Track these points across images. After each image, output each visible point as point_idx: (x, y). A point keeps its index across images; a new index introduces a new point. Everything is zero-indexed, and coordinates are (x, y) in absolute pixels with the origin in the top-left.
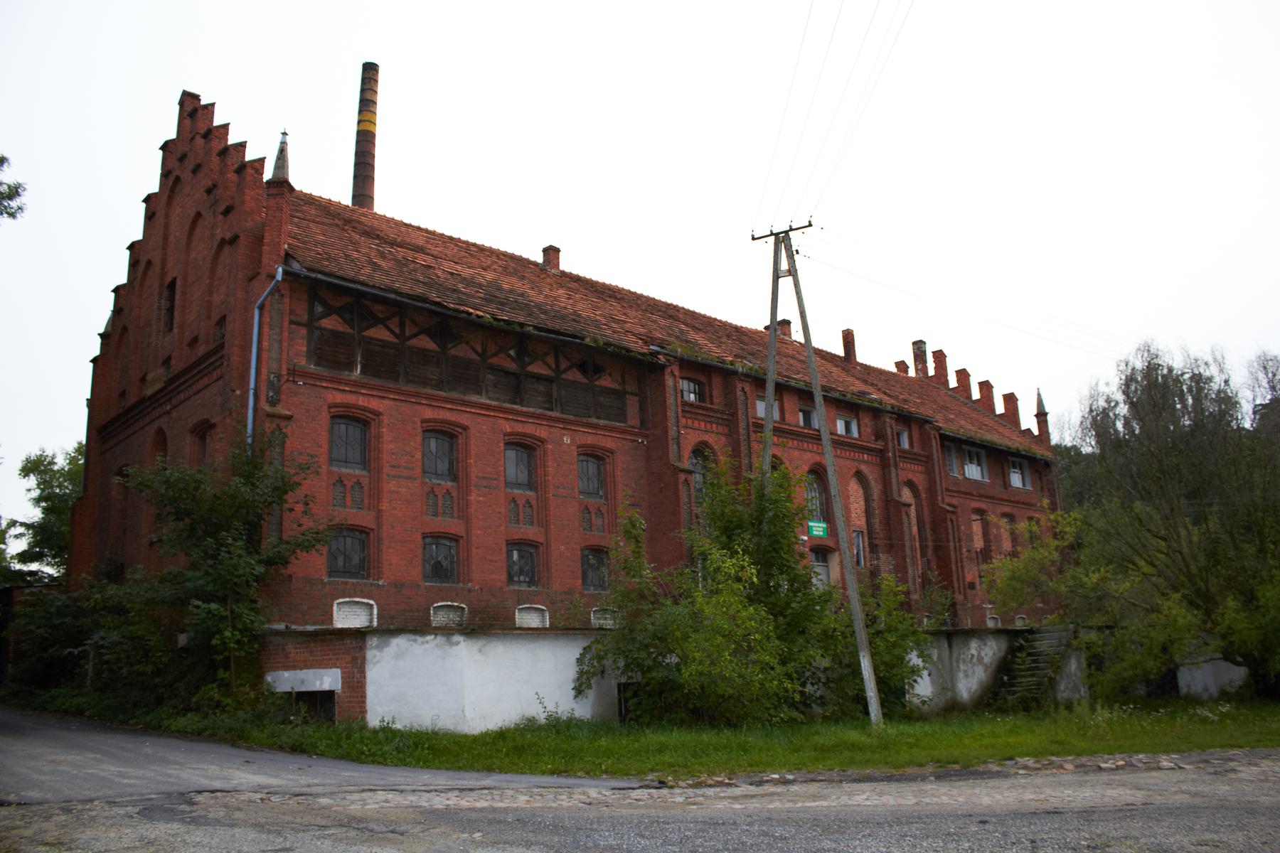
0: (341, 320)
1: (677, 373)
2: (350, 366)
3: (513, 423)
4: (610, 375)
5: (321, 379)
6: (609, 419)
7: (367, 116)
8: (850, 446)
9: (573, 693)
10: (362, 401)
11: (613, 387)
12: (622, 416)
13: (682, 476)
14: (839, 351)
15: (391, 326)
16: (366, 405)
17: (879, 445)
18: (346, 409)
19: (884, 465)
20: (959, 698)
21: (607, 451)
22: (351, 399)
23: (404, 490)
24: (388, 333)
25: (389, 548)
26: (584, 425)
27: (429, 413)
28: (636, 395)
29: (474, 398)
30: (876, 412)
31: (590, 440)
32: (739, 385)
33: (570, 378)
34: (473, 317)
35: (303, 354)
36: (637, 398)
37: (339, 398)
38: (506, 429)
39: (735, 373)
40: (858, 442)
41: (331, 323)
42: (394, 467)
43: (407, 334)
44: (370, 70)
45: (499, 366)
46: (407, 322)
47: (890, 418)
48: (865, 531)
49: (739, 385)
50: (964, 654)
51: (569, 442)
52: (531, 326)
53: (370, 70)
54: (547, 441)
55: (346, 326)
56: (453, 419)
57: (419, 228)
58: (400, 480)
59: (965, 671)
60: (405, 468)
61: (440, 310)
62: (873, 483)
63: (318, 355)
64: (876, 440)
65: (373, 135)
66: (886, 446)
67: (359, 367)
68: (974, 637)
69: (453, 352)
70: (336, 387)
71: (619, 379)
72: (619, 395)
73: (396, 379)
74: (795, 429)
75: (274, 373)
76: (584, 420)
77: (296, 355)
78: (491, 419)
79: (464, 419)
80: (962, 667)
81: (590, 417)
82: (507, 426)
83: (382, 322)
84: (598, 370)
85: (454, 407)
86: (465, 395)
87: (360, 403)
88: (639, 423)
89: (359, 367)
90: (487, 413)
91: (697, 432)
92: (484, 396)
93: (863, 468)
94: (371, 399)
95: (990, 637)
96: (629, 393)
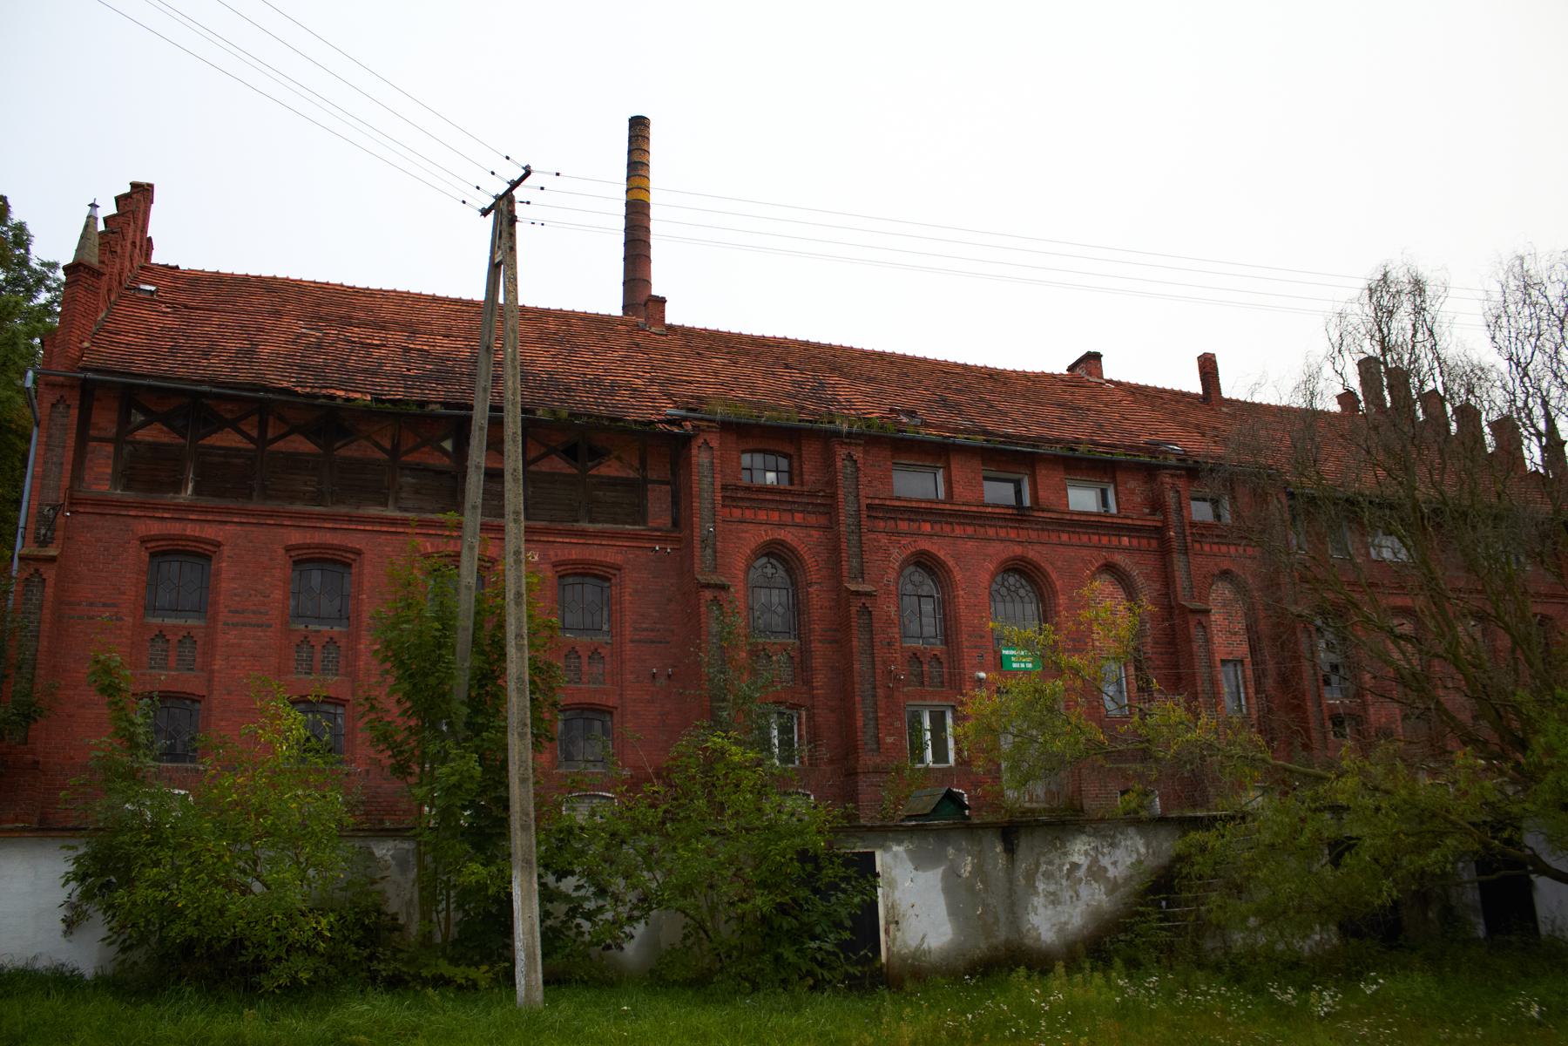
0: (165, 429)
1: (715, 444)
2: (177, 486)
3: (437, 541)
4: (619, 458)
5: (127, 505)
6: (615, 521)
7: (637, 182)
8: (1081, 526)
9: (63, 926)
10: (191, 530)
11: (624, 475)
12: (639, 515)
13: (708, 594)
14: (1195, 387)
15: (245, 428)
16: (197, 534)
17: (1155, 521)
18: (171, 542)
19: (1164, 551)
20: (1028, 942)
21: (608, 567)
22: (175, 528)
23: (251, 641)
24: (238, 437)
25: (222, 720)
26: (560, 533)
27: (296, 537)
28: (667, 483)
29: (374, 511)
30: (1150, 472)
31: (575, 554)
32: (842, 452)
33: (543, 469)
34: (339, 401)
35: (108, 477)
36: (669, 487)
37: (156, 528)
38: (426, 548)
39: (837, 434)
40: (1103, 519)
41: (151, 434)
42: (237, 612)
43: (270, 435)
44: (639, 127)
45: (418, 464)
46: (271, 420)
47: (1172, 476)
48: (1248, 660)
49: (842, 452)
50: (1050, 863)
51: (536, 558)
52: (436, 403)
53: (639, 127)
54: (497, 561)
55: (174, 435)
56: (335, 542)
57: (434, 299)
58: (244, 628)
59: (1049, 894)
60: (254, 612)
61: (291, 399)
62: (1140, 581)
63: (128, 476)
64: (1153, 512)
65: (646, 205)
66: (1165, 521)
67: (190, 486)
68: (1081, 831)
69: (342, 452)
70: (151, 514)
71: (636, 464)
72: (637, 487)
73: (249, 497)
74: (964, 508)
75: (50, 505)
76: (568, 526)
77: (96, 479)
78: (401, 538)
79: (355, 541)
80: (1041, 886)
81: (577, 521)
82: (428, 544)
83: (234, 425)
84: (597, 455)
85: (338, 526)
86: (358, 508)
87: (188, 532)
88: (670, 521)
89: (190, 486)
90: (393, 529)
91: (764, 527)
92: (391, 507)
93: (1119, 559)
94: (206, 526)
95: (1131, 831)
96: (654, 482)
